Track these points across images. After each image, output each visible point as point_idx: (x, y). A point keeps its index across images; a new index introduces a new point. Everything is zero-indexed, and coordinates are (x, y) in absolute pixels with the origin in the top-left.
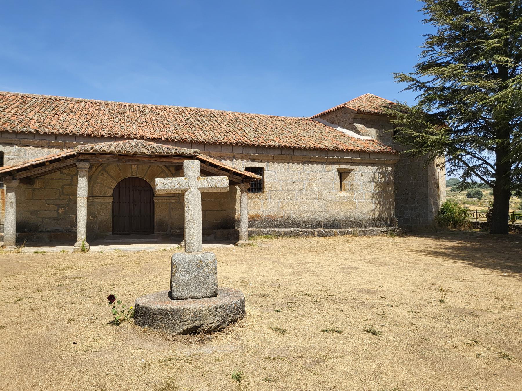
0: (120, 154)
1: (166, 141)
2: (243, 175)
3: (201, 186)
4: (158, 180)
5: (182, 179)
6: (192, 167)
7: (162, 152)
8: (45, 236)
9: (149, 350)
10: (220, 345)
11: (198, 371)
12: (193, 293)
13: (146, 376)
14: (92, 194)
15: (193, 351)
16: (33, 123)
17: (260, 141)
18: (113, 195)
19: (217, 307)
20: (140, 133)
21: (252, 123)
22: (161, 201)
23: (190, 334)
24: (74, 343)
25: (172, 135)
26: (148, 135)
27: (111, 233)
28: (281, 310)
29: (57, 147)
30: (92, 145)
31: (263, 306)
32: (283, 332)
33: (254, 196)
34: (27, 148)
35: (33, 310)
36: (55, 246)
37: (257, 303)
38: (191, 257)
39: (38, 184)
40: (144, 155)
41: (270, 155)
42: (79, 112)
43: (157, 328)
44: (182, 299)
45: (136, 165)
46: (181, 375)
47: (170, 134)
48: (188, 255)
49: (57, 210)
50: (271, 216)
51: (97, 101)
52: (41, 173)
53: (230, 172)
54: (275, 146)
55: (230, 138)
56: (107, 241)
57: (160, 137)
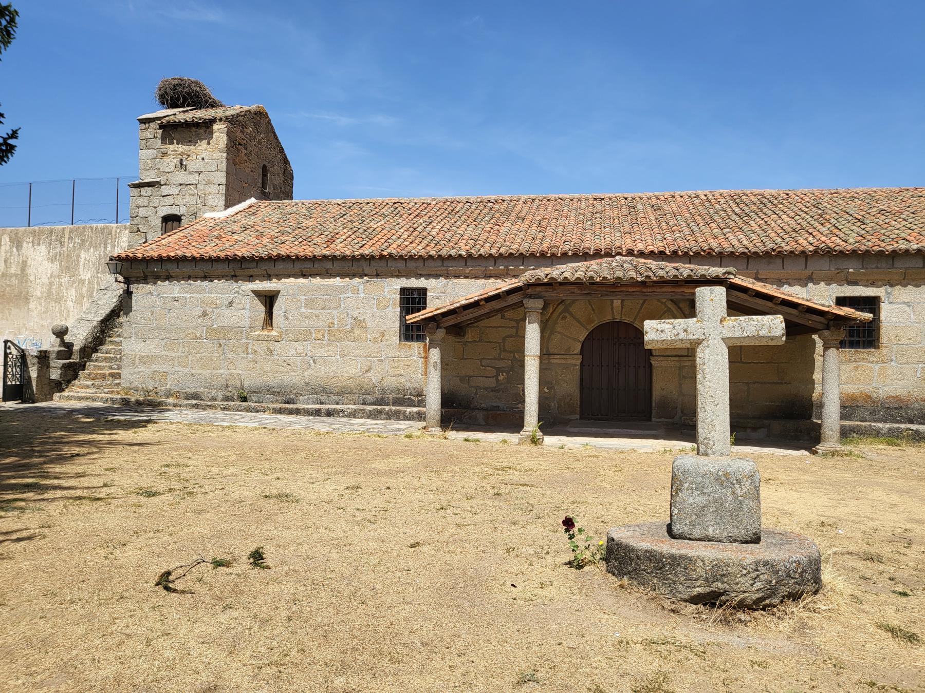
0: (592, 283)
1: (674, 256)
2: (828, 312)
3: (729, 335)
4: (648, 325)
5: (691, 321)
6: (712, 300)
7: (665, 276)
8: (480, 415)
9: (625, 620)
10: (765, 636)
11: (716, 674)
12: (711, 531)
13: (622, 661)
14: (547, 350)
15: (708, 638)
16: (464, 241)
17: (872, 243)
18: (582, 352)
19: (757, 563)
20: (628, 243)
21: (852, 207)
22: (664, 364)
23: (704, 605)
24: (513, 585)
25: (683, 245)
26: (641, 246)
27: (578, 416)
28: (908, 592)
29: (496, 277)
30: (548, 270)
31: (866, 579)
32: (912, 638)
33: (856, 356)
34: (456, 281)
35: (458, 525)
36: (493, 432)
37: (853, 569)
38: (710, 464)
39: (470, 335)
40: (633, 283)
41: (894, 270)
42: (530, 217)
43: (643, 584)
44: (690, 539)
45: (619, 301)
46: (683, 675)
47: (681, 243)
48: (702, 460)
49: (497, 376)
50: (899, 399)
51: (557, 196)
52: (475, 318)
53: (800, 308)
54: (907, 251)
55: (801, 241)
56: (572, 430)
57: (662, 249)
